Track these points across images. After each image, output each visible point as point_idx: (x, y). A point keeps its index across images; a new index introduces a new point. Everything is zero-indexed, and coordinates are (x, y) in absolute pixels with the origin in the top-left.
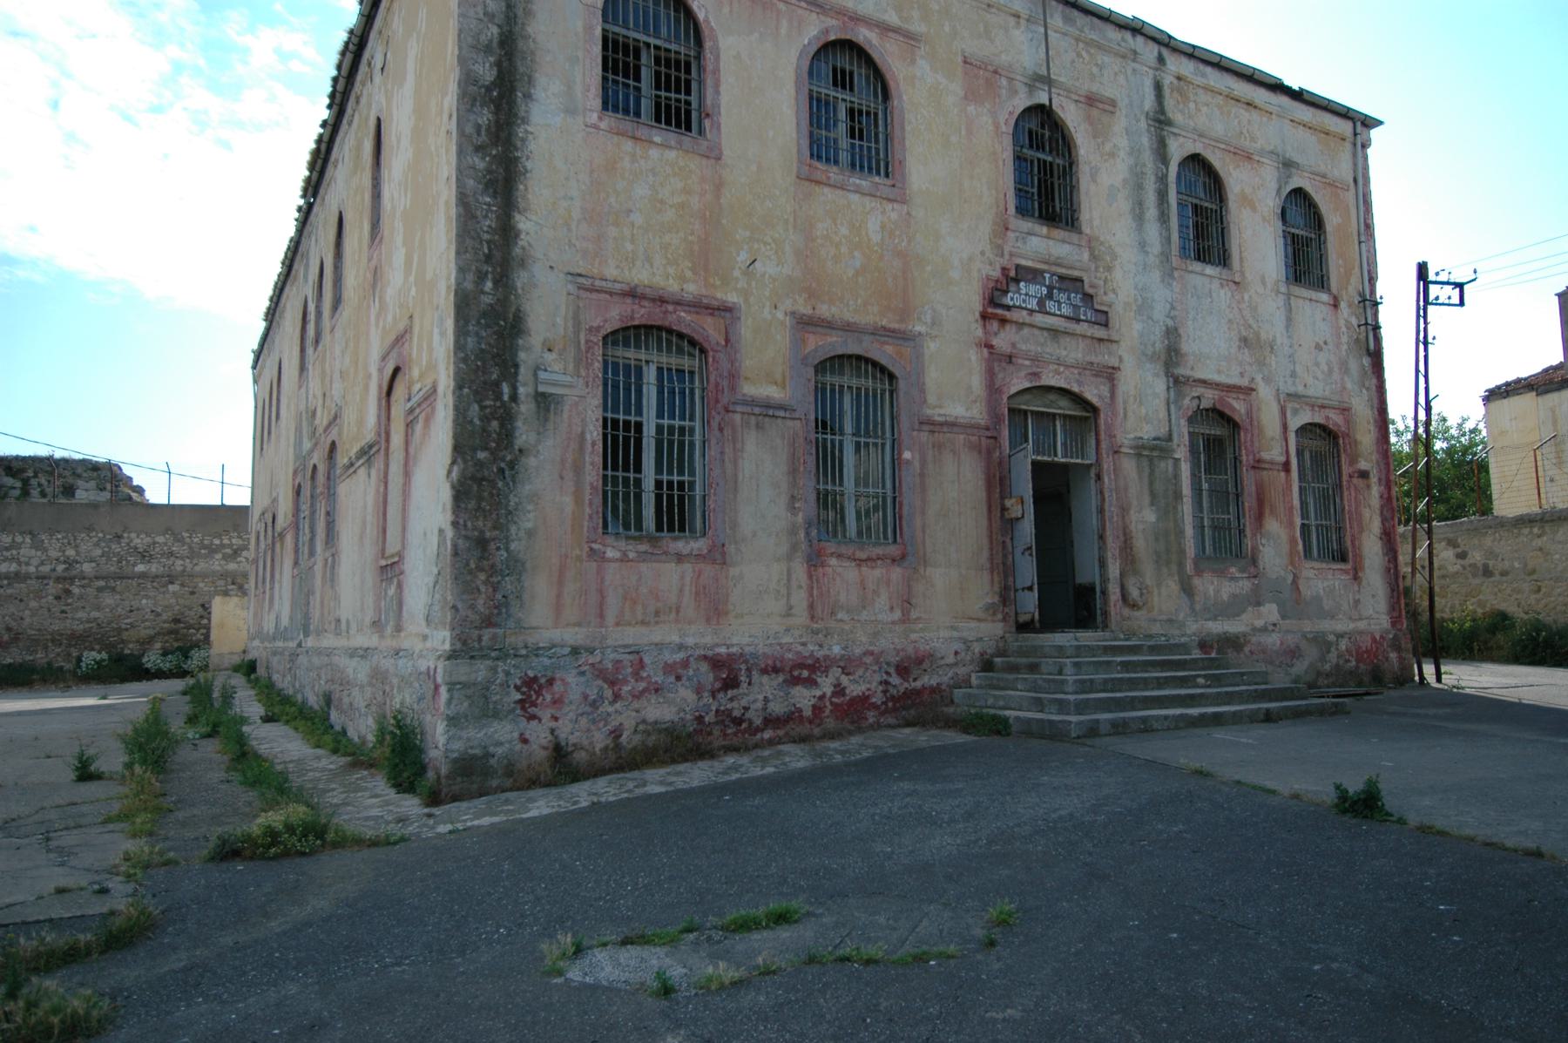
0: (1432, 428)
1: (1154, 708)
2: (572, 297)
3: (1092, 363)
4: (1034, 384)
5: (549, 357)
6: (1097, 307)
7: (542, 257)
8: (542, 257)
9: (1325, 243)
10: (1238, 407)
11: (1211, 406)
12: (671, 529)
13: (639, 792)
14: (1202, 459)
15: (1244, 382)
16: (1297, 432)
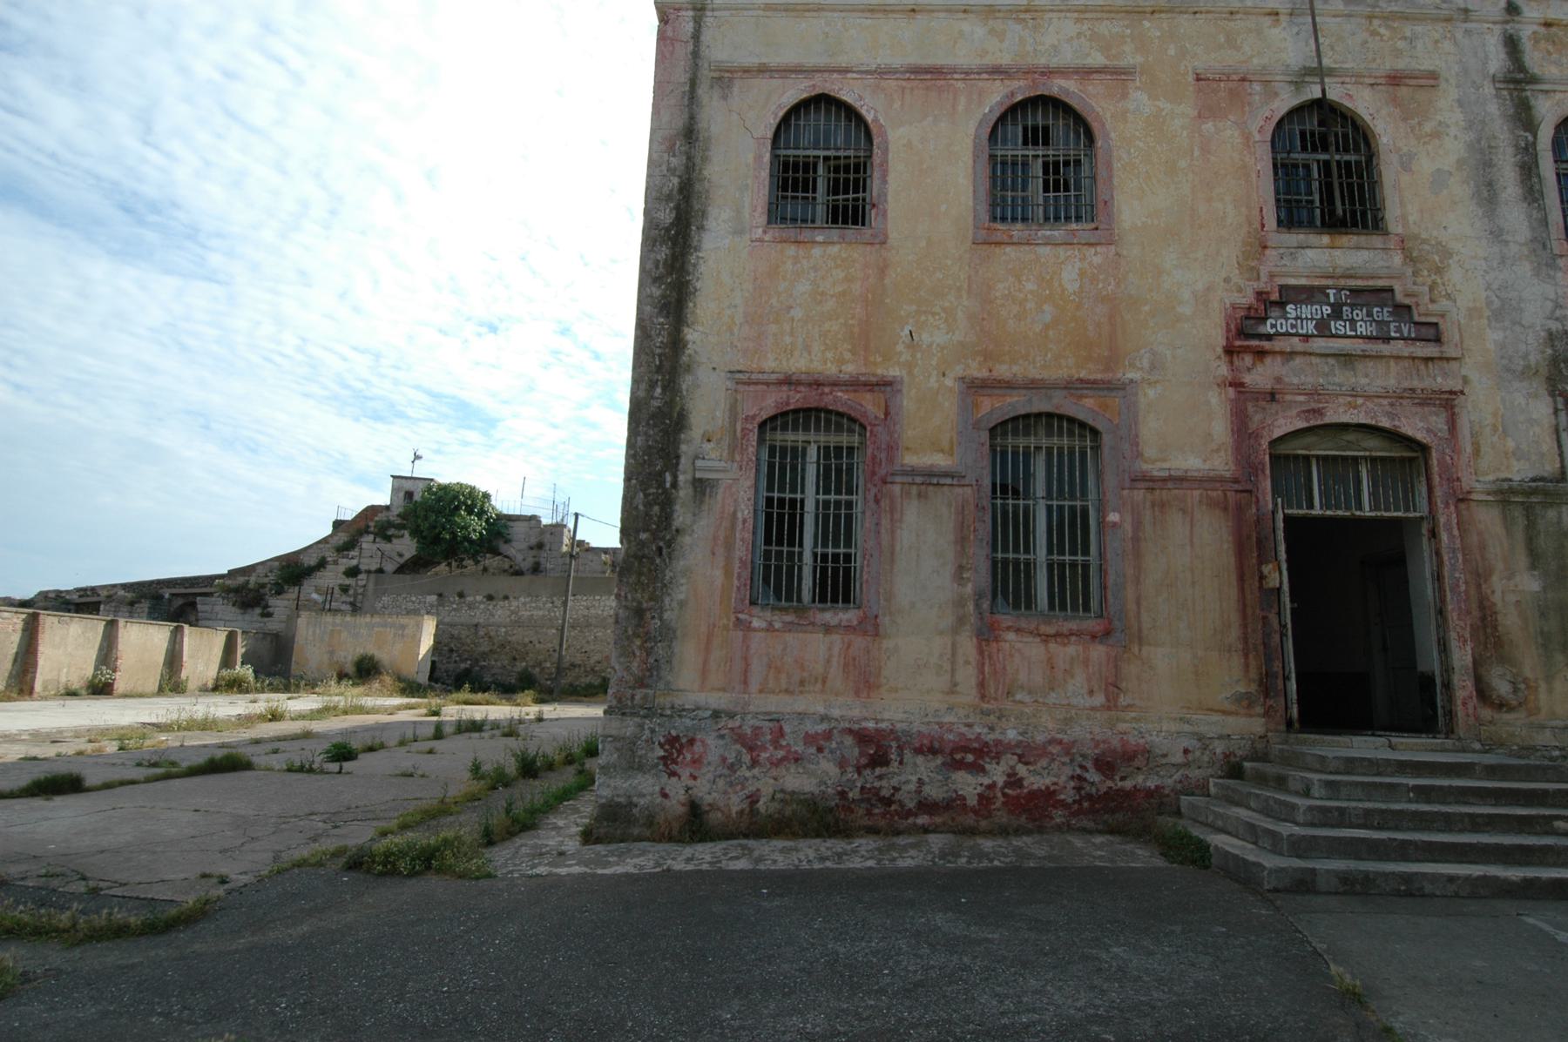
3: (1413, 390)
4: (1313, 423)
6: (1416, 318)
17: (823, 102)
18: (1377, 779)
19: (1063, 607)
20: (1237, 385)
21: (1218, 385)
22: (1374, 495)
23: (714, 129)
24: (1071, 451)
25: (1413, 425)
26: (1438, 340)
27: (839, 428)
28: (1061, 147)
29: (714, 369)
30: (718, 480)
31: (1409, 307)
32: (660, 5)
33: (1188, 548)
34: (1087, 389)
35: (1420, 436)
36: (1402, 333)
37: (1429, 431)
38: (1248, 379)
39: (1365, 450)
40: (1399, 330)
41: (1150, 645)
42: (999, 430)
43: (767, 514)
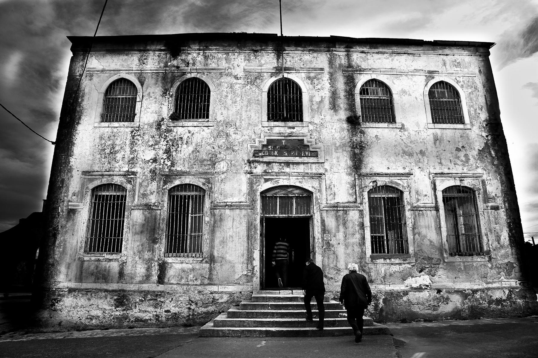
0: (379, 90)
1: (302, 309)
2: (82, 179)
3: (308, 173)
4: (276, 185)
5: (74, 197)
6: (311, 150)
7: (75, 168)
8: (75, 168)
9: (461, 102)
10: (401, 183)
11: (384, 184)
12: (109, 251)
13: (72, 338)
14: (479, 246)
15: (407, 171)
16: (443, 191)
17: (122, 80)
18: (291, 303)
19: (113, 251)
20: (251, 173)
21: (245, 173)
22: (297, 209)
23: (86, 91)
24: (196, 196)
25: (308, 185)
26: (317, 156)
27: (119, 191)
28: (128, 94)
29: (78, 171)
30: (76, 209)
31: (308, 146)
32: (528, 52)
33: (232, 229)
34: (202, 175)
35: (310, 189)
36: (306, 154)
37: (313, 187)
38: (254, 171)
39: (294, 194)
40: (305, 154)
41: (217, 263)
42: (95, 190)
43: (93, 220)
